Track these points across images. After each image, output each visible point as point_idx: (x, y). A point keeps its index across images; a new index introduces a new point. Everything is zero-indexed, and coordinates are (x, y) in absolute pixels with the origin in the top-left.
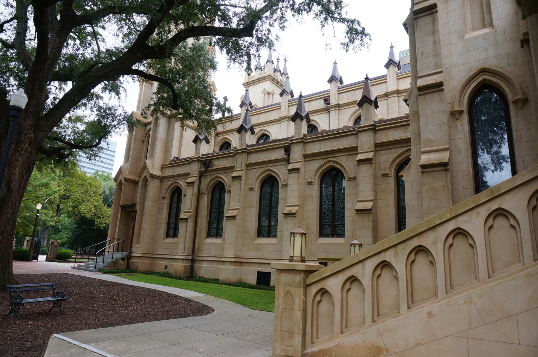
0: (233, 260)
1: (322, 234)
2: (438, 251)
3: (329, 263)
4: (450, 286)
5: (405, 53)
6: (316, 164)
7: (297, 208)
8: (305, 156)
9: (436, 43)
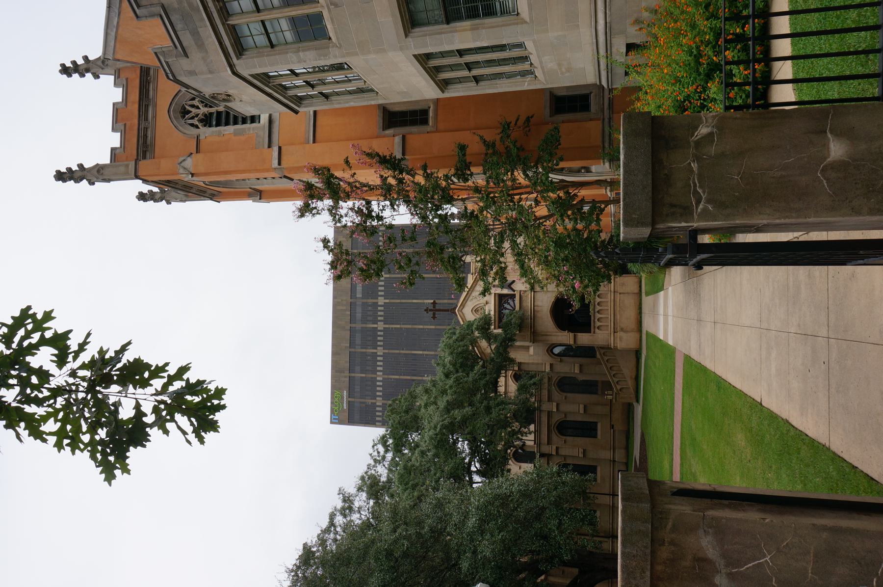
0: (610, 585)
1: (595, 436)
2: (611, 365)
3: (612, 423)
4: (618, 363)
5: (333, 417)
6: (555, 437)
7: (580, 449)
8: (548, 444)
9: (533, 364)
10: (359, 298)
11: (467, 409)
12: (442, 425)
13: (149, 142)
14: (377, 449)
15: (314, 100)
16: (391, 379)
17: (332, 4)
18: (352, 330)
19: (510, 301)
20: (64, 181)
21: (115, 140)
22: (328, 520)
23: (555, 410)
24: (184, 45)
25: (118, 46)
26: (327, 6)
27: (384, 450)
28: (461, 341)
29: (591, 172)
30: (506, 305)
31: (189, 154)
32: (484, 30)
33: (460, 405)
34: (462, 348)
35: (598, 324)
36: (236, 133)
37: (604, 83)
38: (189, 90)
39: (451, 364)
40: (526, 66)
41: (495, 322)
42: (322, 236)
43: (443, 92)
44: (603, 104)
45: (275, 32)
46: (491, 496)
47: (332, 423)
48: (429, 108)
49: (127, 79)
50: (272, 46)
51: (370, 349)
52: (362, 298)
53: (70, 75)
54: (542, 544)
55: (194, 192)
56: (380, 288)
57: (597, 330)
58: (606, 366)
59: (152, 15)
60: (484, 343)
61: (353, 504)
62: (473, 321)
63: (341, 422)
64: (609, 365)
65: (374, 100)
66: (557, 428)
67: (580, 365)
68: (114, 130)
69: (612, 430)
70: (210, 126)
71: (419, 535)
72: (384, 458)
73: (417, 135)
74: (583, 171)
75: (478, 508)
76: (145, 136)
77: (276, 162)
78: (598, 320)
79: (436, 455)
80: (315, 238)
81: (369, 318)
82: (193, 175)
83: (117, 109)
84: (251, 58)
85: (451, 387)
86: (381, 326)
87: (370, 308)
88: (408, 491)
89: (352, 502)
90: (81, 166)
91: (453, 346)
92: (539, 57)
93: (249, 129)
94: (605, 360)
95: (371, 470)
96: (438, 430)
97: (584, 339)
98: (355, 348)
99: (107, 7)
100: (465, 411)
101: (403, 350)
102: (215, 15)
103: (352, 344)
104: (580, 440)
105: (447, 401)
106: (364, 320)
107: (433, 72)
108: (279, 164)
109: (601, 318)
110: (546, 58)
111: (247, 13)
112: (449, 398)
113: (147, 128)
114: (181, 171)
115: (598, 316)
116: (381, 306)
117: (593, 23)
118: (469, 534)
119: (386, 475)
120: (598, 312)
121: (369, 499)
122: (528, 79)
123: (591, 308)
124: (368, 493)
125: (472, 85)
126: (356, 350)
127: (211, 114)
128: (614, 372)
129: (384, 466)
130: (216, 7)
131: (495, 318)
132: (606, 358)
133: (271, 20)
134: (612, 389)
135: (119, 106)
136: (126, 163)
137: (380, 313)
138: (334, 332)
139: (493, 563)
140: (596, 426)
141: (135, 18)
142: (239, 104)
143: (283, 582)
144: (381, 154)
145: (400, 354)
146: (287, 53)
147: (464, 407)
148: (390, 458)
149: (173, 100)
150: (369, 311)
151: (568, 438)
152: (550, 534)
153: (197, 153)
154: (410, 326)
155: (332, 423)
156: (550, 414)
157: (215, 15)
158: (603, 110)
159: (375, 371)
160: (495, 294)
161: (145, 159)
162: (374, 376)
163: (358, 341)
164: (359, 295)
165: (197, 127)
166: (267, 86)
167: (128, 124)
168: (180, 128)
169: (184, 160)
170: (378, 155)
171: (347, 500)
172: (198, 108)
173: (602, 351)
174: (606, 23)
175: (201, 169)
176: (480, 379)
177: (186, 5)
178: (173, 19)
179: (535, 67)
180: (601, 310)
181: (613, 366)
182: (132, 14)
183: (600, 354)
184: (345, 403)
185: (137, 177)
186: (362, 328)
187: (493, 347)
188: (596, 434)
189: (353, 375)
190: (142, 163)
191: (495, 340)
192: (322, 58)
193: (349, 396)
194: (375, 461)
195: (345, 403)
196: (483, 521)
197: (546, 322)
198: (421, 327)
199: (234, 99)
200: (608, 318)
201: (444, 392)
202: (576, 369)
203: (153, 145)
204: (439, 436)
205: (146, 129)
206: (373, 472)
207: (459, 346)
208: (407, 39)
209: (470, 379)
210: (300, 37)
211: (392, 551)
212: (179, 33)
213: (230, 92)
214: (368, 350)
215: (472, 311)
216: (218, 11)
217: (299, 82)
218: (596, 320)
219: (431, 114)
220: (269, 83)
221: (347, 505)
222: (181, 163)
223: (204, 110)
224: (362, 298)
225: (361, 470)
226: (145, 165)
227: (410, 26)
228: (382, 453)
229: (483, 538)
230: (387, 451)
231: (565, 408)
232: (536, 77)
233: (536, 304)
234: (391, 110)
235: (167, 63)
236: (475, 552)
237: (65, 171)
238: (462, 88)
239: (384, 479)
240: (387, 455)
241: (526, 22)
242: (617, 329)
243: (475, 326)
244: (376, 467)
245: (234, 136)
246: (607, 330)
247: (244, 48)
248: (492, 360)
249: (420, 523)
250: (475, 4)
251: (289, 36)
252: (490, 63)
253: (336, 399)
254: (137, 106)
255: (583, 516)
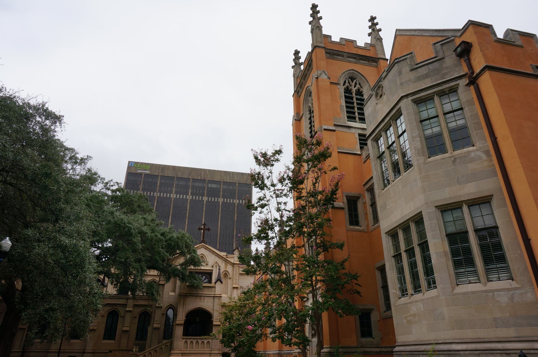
5: (133, 163)
6: (107, 308)
7: (96, 327)
10: (208, 186)
11: (141, 246)
12: (131, 228)
13: (335, 56)
14: (115, 185)
15: (376, 150)
16: (154, 201)
17: (455, 159)
18: (188, 180)
19: (207, 280)
20: (312, 9)
21: (336, 38)
22: (69, 147)
23: (127, 309)
24: (418, 69)
25: (407, 37)
26: (453, 156)
27: (114, 189)
28: (185, 245)
29: (312, 338)
30: (204, 277)
31: (330, 77)
32: (445, 260)
33: (143, 242)
34: (181, 245)
35: (189, 341)
36: (341, 106)
37: (397, 349)
38: (385, 72)
39: (171, 237)
40: (410, 290)
41: (195, 269)
42: (283, 151)
43: (386, 233)
44: (366, 347)
45: (430, 124)
46: (84, 255)
47: (129, 162)
48: (360, 227)
49: (369, 50)
50: (421, 121)
51: (175, 190)
52: (208, 187)
53: (370, 21)
54: (39, 295)
55: (302, 81)
56: (213, 198)
57: (184, 341)
58: (158, 347)
59: (436, 52)
60: (182, 260)
61: (78, 165)
62: (197, 254)
63: (129, 168)
64: (158, 350)
65: (378, 187)
66: (114, 311)
67: (159, 328)
68: (341, 39)
69: (108, 351)
70: (345, 92)
71: (59, 200)
72: (109, 189)
73: (344, 216)
74: (313, 332)
75: (75, 245)
76: (339, 55)
77: (326, 127)
78: (192, 342)
79: (109, 222)
80: (282, 146)
81: (195, 190)
82: (317, 78)
83: (353, 42)
84: (413, 108)
85: (156, 236)
86: (189, 197)
87: (201, 191)
88: (86, 200)
89: (80, 164)
90: (321, 18)
91: (183, 239)
92: (422, 300)
93: (344, 115)
94: (162, 347)
95: (101, 180)
96: (128, 225)
97: (179, 331)
98: (177, 180)
99: (436, 29)
100: (139, 244)
101: (173, 210)
102: (440, 88)
103: (179, 179)
104: (103, 326)
105: (147, 233)
106: (193, 187)
107: (405, 227)
108: (325, 129)
109: (193, 344)
110: (421, 305)
111: (442, 108)
112: (149, 234)
113: (343, 56)
114: (319, 72)
115: (195, 342)
116: (202, 198)
117: (457, 341)
118: (55, 237)
119: (95, 190)
120: (197, 342)
121: (81, 176)
122: (397, 292)
123: (207, 337)
124: (86, 175)
125: (392, 253)
126: (175, 181)
127: (352, 94)
128: (152, 353)
129: (102, 189)
130: (446, 88)
131: (199, 269)
132: (163, 347)
133: (439, 121)
134: (140, 351)
135: (354, 43)
136: (323, 42)
137: (197, 197)
138: (188, 168)
139: (27, 254)
140: (112, 339)
141: (434, 43)
142: (375, 103)
143: (35, 99)
144: (337, 192)
145: (170, 208)
146: (418, 130)
147: (142, 244)
148: (108, 193)
149: (359, 73)
150: (200, 191)
151: (105, 318)
152: (45, 302)
153: (330, 82)
154: (187, 215)
155: (129, 162)
156: (125, 305)
157: (440, 88)
158: (362, 347)
159: (160, 192)
160: (212, 270)
161: (326, 53)
162: (157, 191)
163: (181, 183)
164: (210, 185)
165: (344, 85)
166: (390, 119)
167: (345, 47)
168: (344, 75)
169: (326, 74)
170: (337, 190)
171: (83, 161)
172: (355, 87)
173: (168, 344)
174: (459, 351)
175: (320, 84)
176: (160, 256)
177: (445, 71)
178: (436, 63)
179: (410, 298)
180: (198, 344)
181: (157, 353)
182: (435, 42)
183: (167, 343)
184: (141, 171)
185: (314, 47)
186: (189, 186)
187: (179, 267)
188: (106, 339)
189: (159, 178)
190: (323, 51)
191: (183, 269)
192: (417, 152)
193: (145, 174)
194: (107, 183)
195: (141, 171)
196: (63, 248)
197: (193, 304)
198: (187, 223)
199: (378, 100)
200: (187, 349)
201: (153, 231)
202: (156, 325)
203: (333, 59)
204: (123, 225)
205: (343, 56)
206: (100, 181)
207: (183, 244)
208: (434, 207)
209: (161, 250)
210: (428, 139)
211: (50, 178)
212: (426, 67)
213: (384, 97)
214: (174, 188)
215: (202, 254)
216: (443, 90)
217: (393, 138)
218: (192, 340)
219: (356, 227)
220: (392, 120)
221: (78, 161)
222: (324, 72)
223: (354, 90)
224: (208, 187)
225: (102, 173)
226: (321, 53)
227: (443, 209)
228: (112, 188)
229: (50, 248)
230: (113, 191)
231: (128, 316)
232: (400, 298)
233: (206, 297)
234: (358, 202)
235: (406, 59)
236: (39, 241)
237: (317, 10)
238: (389, 246)
239: (93, 188)
240: (109, 191)
241: (453, 291)
242: (185, 355)
243: (194, 255)
244: (102, 184)
245: (340, 105)
246: (184, 349)
247: (418, 105)
248: (170, 266)
249: (67, 202)
250: (462, 255)
251: (428, 132)
252: (413, 266)
253: (144, 166)
254: (355, 53)
255: (58, 329)
